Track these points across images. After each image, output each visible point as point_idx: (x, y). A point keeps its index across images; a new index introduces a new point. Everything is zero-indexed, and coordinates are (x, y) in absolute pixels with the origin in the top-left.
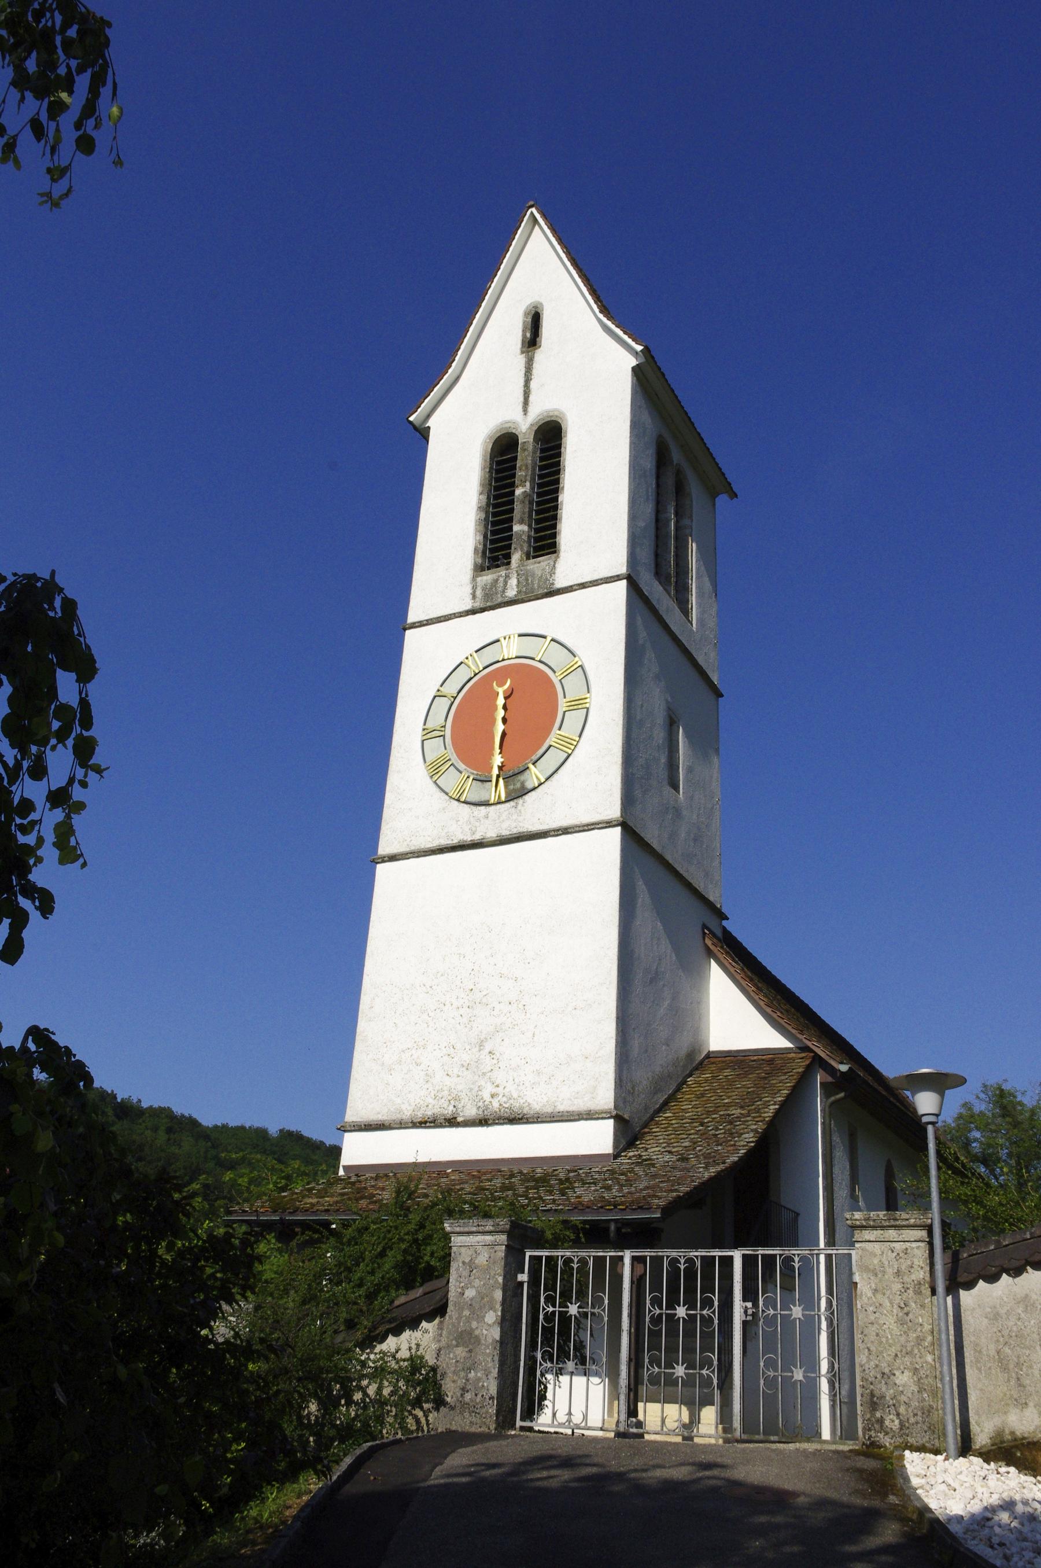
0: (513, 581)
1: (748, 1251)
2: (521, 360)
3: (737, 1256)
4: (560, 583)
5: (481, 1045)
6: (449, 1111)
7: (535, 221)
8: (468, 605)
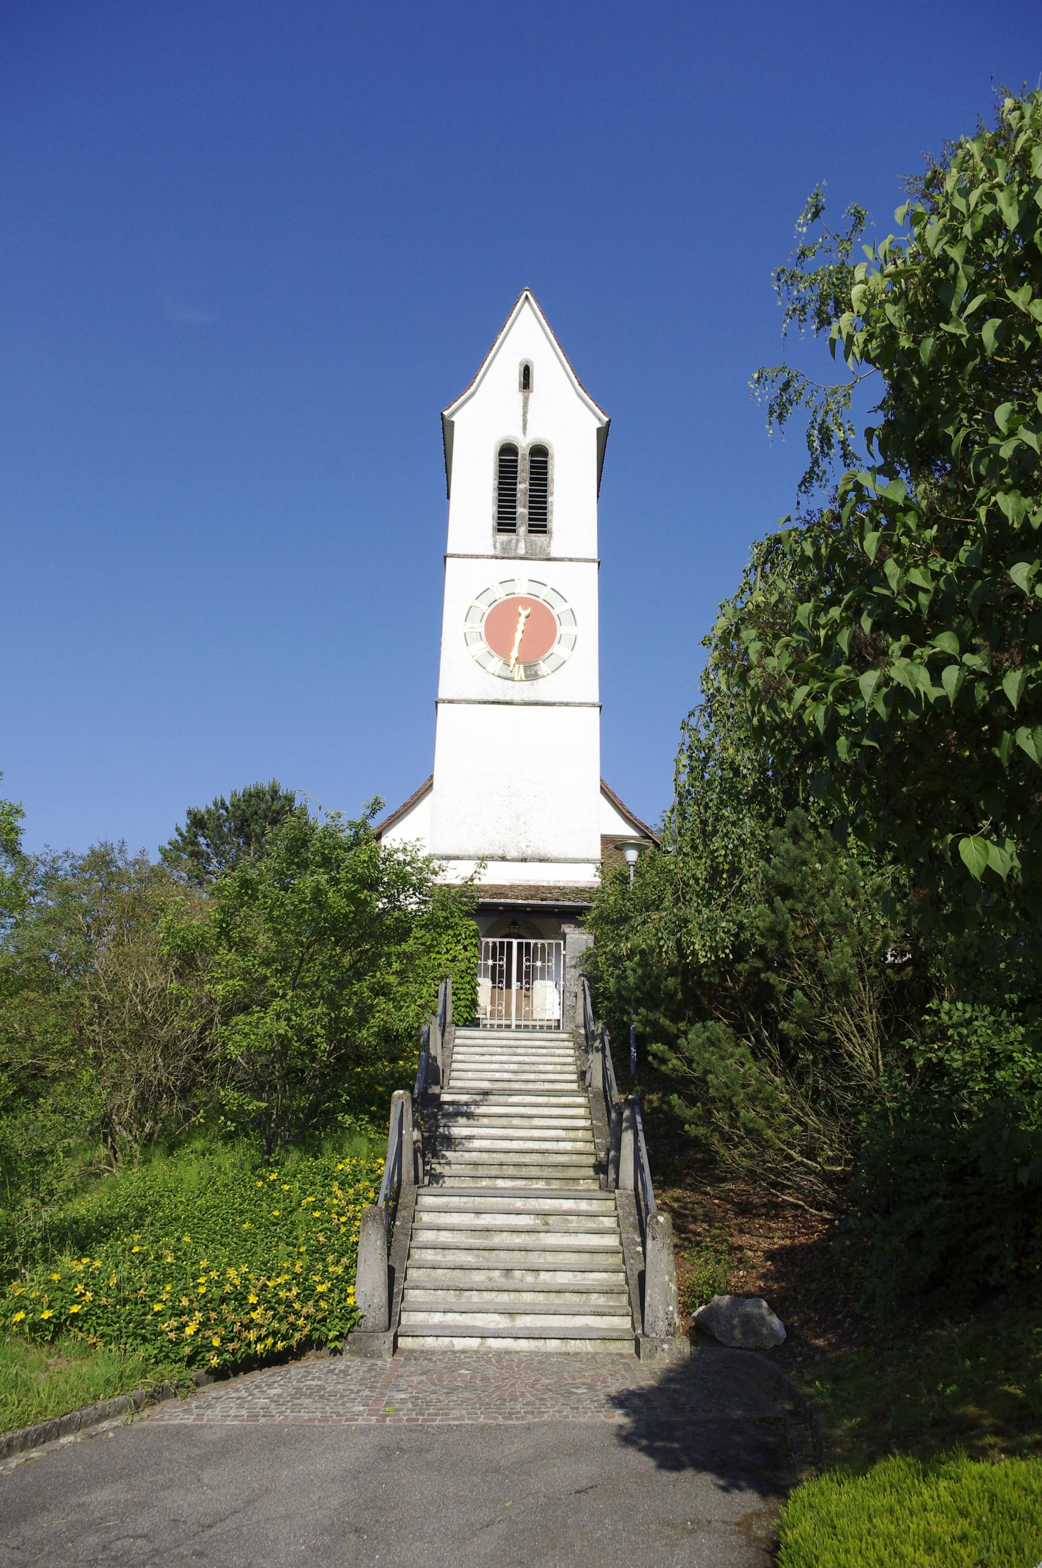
0: (522, 545)
1: (520, 940)
2: (519, 396)
3: (515, 942)
4: (553, 555)
5: (518, 818)
6: (500, 853)
7: (527, 297)
8: (491, 552)
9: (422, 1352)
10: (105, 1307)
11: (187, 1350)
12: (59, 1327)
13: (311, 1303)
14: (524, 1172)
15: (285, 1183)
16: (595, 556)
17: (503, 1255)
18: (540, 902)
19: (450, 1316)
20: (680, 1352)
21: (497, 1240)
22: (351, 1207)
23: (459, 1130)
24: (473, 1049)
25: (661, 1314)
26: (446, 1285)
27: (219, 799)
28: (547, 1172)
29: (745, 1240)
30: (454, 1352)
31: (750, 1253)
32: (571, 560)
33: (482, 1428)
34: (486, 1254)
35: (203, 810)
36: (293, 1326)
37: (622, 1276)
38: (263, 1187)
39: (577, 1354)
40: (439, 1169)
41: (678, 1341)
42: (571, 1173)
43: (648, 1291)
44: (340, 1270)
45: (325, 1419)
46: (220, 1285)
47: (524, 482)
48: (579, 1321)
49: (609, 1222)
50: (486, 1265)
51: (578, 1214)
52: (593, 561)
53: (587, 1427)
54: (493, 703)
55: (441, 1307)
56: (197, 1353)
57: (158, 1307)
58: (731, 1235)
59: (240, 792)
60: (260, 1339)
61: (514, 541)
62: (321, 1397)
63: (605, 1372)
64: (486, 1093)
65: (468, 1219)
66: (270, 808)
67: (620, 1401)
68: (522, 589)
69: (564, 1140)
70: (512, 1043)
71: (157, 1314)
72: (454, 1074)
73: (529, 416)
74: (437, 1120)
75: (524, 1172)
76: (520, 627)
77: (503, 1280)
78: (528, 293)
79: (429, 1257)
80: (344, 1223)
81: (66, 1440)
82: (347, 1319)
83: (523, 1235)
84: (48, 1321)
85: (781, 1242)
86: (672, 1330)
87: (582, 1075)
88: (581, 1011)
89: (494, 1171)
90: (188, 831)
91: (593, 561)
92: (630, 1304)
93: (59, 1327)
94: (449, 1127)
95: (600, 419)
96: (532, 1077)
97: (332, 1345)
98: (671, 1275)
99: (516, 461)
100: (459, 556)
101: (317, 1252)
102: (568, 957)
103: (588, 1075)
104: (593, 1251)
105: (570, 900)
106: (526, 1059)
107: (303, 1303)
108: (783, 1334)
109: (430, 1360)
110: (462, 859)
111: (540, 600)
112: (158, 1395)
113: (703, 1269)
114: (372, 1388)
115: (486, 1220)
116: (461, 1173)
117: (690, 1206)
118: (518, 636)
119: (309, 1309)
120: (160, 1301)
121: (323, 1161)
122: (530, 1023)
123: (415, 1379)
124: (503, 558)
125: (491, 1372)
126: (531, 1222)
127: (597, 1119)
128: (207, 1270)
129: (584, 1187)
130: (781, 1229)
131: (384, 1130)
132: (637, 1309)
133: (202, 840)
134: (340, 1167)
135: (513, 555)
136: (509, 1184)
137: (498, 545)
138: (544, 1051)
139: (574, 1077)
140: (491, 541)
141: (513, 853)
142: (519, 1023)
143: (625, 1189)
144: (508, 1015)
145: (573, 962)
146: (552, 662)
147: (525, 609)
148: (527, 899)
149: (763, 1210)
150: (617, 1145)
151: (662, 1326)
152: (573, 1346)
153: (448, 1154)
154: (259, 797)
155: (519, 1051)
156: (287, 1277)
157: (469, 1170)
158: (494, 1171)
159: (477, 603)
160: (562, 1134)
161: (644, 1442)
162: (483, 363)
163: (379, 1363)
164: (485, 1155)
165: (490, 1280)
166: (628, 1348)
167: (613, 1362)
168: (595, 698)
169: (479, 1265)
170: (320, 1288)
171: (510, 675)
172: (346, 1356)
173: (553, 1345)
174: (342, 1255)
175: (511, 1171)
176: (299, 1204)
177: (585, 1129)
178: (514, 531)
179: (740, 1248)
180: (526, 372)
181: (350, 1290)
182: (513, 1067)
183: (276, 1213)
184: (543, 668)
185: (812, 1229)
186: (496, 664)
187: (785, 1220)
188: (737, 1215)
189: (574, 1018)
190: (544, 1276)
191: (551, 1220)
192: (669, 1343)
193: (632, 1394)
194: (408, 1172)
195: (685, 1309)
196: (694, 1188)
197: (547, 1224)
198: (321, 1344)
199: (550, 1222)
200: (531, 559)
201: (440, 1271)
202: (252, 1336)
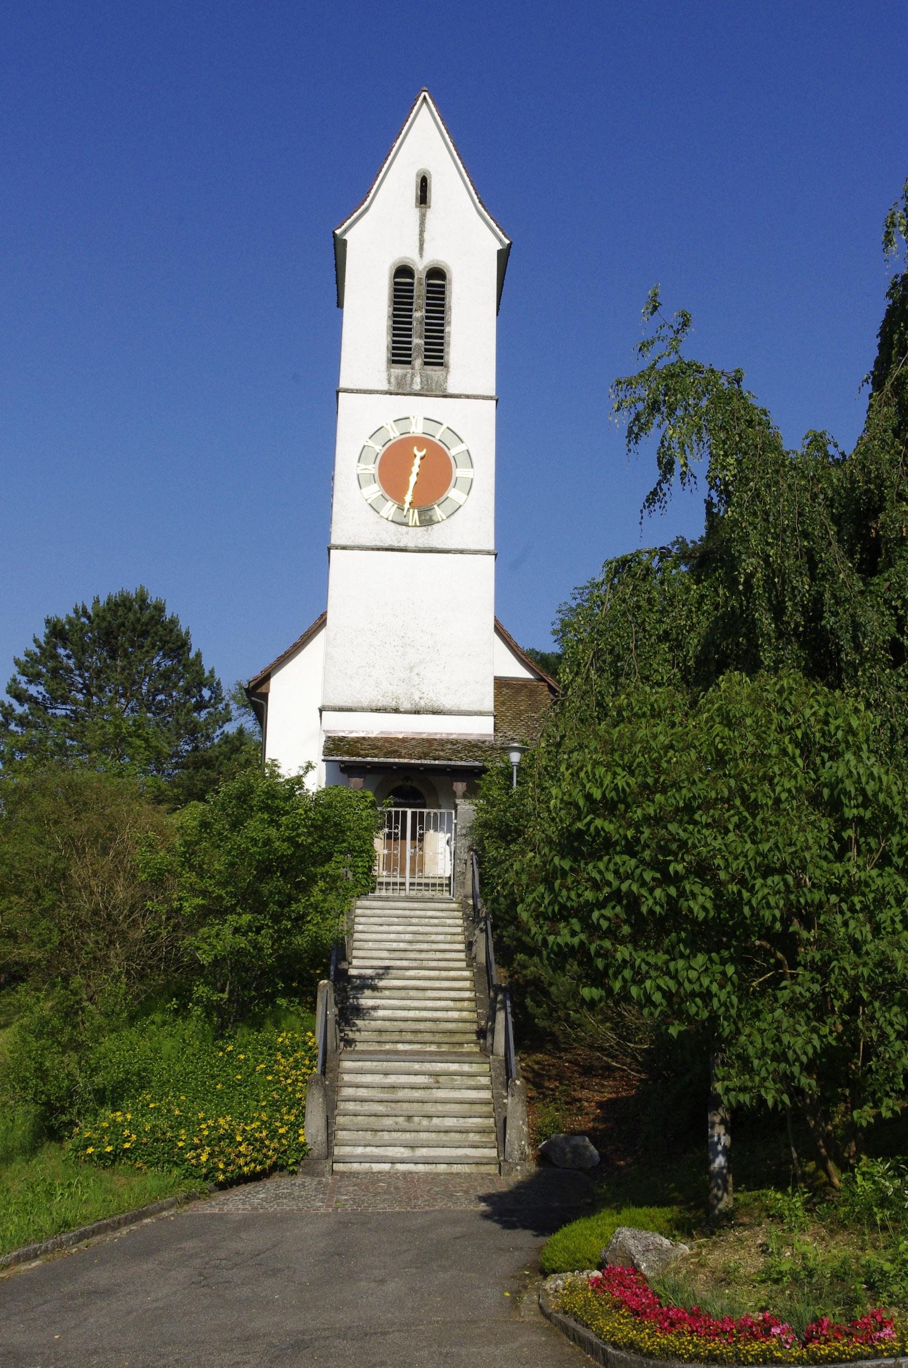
0: (417, 379)
1: (414, 810)
2: (414, 213)
3: (409, 811)
4: (451, 390)
5: (411, 669)
6: (393, 704)
7: (425, 98)
8: (385, 387)
9: (351, 1173)
10: (146, 1144)
11: (204, 1171)
12: (115, 1157)
13: (276, 1140)
14: (419, 1037)
15: (240, 1053)
16: (493, 393)
17: (405, 1105)
18: (433, 762)
19: (368, 1149)
20: (528, 1171)
21: (401, 1094)
22: (293, 1072)
23: (366, 1001)
24: (372, 920)
25: (516, 1147)
26: (365, 1127)
27: (80, 605)
28: (438, 1038)
29: (585, 1093)
30: (372, 1173)
31: (586, 1104)
32: (468, 397)
33: (399, 1213)
34: (393, 1105)
35: (63, 619)
36: (265, 1155)
37: (492, 1120)
38: (223, 1056)
39: (458, 1174)
40: (351, 1035)
41: (527, 1164)
42: (457, 1038)
43: (508, 1131)
44: (292, 1118)
45: (300, 1210)
46: (216, 1128)
47: (420, 309)
48: (460, 1152)
49: (485, 1081)
50: (393, 1113)
51: (461, 1074)
52: (491, 398)
53: (462, 1212)
54: (387, 549)
55: (363, 1143)
56: (209, 1173)
57: (181, 1144)
58: (575, 1090)
59: (103, 600)
60: (246, 1164)
61: (409, 375)
62: (293, 1198)
63: (476, 1184)
64: (388, 968)
65: (378, 1079)
66: (138, 620)
67: (483, 1199)
68: (417, 429)
69: (452, 1010)
70: (407, 913)
71: (181, 1148)
72: (356, 944)
73: (426, 236)
74: (346, 992)
75: (419, 1037)
76: (415, 469)
77: (406, 1124)
78: (426, 94)
79: (351, 1108)
80: (290, 1084)
81: (147, 1221)
82: (300, 1151)
83: (420, 1091)
84: (110, 1153)
85: (610, 1096)
86: (523, 1157)
87: (470, 945)
88: (470, 883)
89: (395, 1037)
90: (47, 643)
91: (491, 398)
92: (497, 1139)
93: (115, 1157)
94: (358, 998)
95: (501, 241)
96: (425, 946)
97: (291, 1168)
98: (524, 1120)
99: (412, 284)
100: (351, 391)
101: (275, 1106)
102: (459, 827)
103: (474, 948)
104: (472, 1103)
105: (461, 759)
106: (420, 929)
107: (272, 1140)
108: (598, 1159)
109: (358, 1178)
110: (355, 711)
111: (436, 440)
112: (189, 1198)
113: (552, 1114)
114: (324, 1194)
115: (392, 1079)
116: (368, 1038)
117: (547, 1068)
118: (413, 479)
119: (275, 1144)
120: (181, 1140)
121: (265, 1035)
122: (423, 881)
123: (351, 1189)
124: (398, 394)
125: (401, 1184)
126: (426, 1081)
127: (480, 992)
128: (204, 1119)
129: (468, 1050)
130: (610, 1086)
131: (313, 1009)
132: (501, 1143)
133: (61, 651)
134: (280, 1040)
135: (408, 390)
136: (407, 1047)
137: (393, 380)
138: (436, 921)
139: (462, 947)
140: (384, 375)
141: (406, 706)
142: (413, 880)
143: (497, 1055)
144: (403, 870)
145: (464, 832)
146: (448, 507)
147: (420, 450)
148: (420, 758)
149: (600, 1072)
150: (492, 1018)
151: (517, 1154)
152: (456, 1168)
153: (357, 1022)
154: (125, 605)
155: (414, 921)
156: (258, 1123)
157: (374, 1036)
158: (395, 1037)
159: (370, 443)
160: (450, 1004)
161: (496, 1218)
162: (378, 175)
163: (324, 1180)
164: (387, 1023)
165: (397, 1123)
166: (493, 1169)
167: (483, 1178)
168: (490, 545)
169: (388, 1113)
170: (281, 1131)
171: (404, 520)
172: (300, 1175)
173: (442, 1168)
174: (291, 1108)
175: (409, 1037)
176: (254, 1070)
177: (469, 1000)
178: (409, 363)
179: (580, 1100)
180: (424, 184)
181: (301, 1132)
182: (408, 937)
183: (239, 1077)
184: (438, 513)
185: (632, 1086)
186: (389, 509)
187: (615, 1079)
188: (581, 1074)
189: (464, 883)
190: (435, 1121)
191: (441, 1079)
192: (521, 1165)
193: (493, 1195)
194: (332, 1043)
195: (534, 1144)
196: (551, 1054)
197: (438, 1082)
198: (282, 1168)
199: (440, 1080)
200: (426, 396)
201: (360, 1118)
202: (241, 1161)
